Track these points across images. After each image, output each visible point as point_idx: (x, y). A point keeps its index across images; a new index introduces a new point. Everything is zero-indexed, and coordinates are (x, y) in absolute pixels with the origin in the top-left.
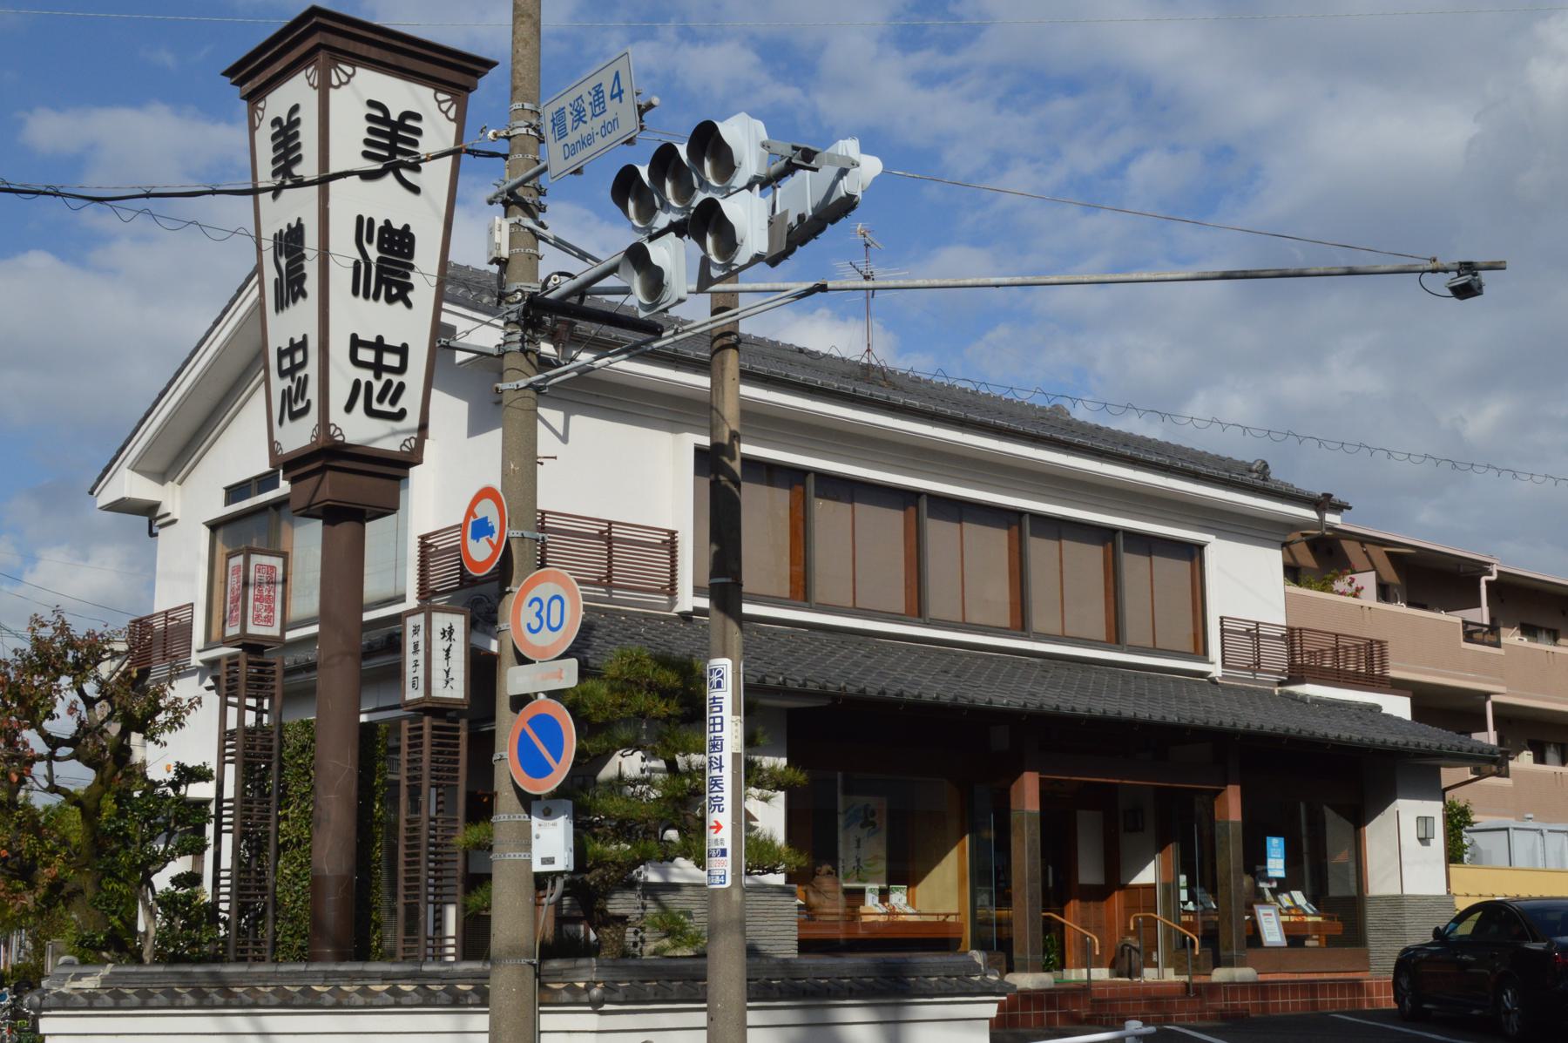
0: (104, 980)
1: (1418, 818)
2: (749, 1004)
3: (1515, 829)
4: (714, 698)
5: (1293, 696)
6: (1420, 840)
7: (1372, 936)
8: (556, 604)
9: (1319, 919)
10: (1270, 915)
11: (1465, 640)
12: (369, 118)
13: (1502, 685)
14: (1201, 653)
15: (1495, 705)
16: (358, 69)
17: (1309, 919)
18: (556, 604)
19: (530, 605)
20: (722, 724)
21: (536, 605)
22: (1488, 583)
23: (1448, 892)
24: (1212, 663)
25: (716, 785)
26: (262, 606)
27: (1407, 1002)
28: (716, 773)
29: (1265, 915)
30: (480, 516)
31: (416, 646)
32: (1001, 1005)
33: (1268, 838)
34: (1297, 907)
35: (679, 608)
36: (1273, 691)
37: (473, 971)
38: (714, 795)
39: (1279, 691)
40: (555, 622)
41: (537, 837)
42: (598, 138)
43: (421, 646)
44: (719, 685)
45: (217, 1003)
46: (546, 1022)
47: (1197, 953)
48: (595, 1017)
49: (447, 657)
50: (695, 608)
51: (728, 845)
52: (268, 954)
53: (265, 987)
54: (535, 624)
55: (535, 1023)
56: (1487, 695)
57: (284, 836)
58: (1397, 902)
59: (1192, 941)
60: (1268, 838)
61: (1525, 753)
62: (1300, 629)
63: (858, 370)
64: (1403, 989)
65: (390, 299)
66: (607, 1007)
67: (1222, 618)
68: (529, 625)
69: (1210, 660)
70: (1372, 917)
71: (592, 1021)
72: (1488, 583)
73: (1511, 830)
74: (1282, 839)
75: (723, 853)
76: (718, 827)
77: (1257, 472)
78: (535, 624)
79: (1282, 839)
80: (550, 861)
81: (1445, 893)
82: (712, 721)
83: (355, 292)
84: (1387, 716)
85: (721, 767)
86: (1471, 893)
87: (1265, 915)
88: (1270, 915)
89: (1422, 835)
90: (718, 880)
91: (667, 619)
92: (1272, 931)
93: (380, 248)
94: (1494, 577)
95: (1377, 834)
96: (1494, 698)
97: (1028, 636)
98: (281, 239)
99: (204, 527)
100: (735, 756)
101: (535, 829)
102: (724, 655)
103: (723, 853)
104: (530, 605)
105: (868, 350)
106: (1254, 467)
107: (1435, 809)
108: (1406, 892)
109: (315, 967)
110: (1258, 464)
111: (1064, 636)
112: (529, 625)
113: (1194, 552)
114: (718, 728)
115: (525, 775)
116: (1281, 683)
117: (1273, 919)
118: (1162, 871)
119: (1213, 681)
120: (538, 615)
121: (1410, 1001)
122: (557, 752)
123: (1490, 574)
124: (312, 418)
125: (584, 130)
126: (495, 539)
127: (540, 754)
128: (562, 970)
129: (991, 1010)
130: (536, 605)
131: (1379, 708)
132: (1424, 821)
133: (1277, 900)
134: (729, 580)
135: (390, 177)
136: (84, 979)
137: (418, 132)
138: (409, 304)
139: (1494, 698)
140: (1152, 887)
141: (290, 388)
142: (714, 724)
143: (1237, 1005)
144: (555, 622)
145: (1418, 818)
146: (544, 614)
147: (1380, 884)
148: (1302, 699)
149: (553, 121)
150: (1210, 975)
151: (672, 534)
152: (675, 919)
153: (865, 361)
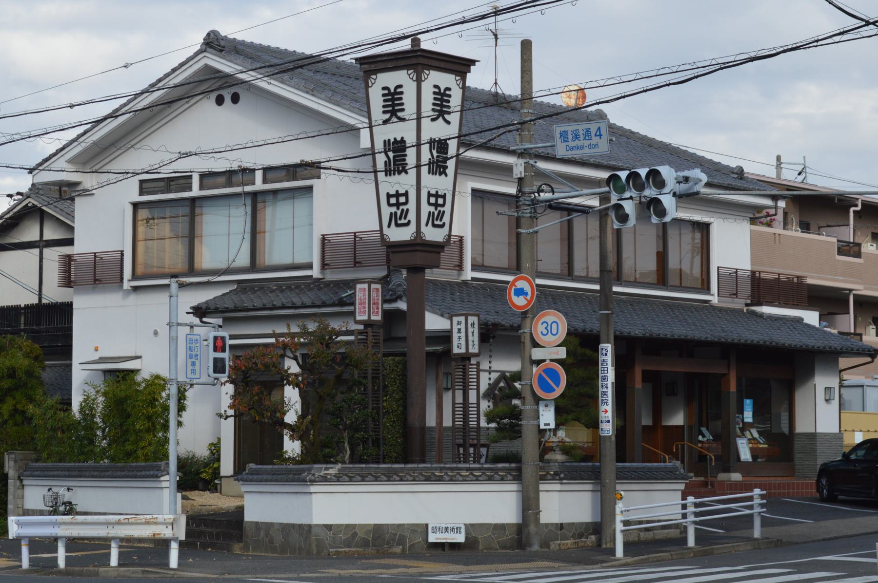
0: (339, 470)
1: (826, 388)
2: (617, 481)
3: (868, 386)
4: (604, 360)
5: (754, 313)
6: (827, 400)
7: (797, 456)
8: (554, 325)
9: (766, 446)
10: (744, 443)
11: (838, 255)
12: (435, 93)
13: (861, 284)
14: (707, 289)
15: (855, 295)
16: (431, 71)
17: (761, 446)
18: (554, 325)
19: (542, 324)
20: (607, 370)
21: (545, 325)
22: (854, 212)
23: (840, 431)
24: (713, 295)
25: (605, 394)
26: (375, 306)
27: (825, 491)
28: (605, 390)
29: (741, 443)
30: (519, 287)
31: (459, 331)
32: (687, 485)
33: (745, 400)
34: (754, 439)
35: (464, 278)
36: (743, 310)
37: (505, 467)
38: (604, 399)
39: (747, 310)
40: (554, 332)
41: (542, 415)
42: (587, 149)
43: (463, 330)
44: (606, 354)
45: (382, 480)
46: (542, 487)
47: (713, 464)
48: (559, 485)
49: (473, 335)
50: (472, 278)
51: (610, 419)
52: (381, 460)
53: (414, 473)
54: (545, 332)
55: (538, 487)
56: (851, 290)
57: (385, 409)
58: (812, 437)
59: (711, 459)
60: (745, 400)
61: (871, 327)
62: (760, 272)
63: (491, 98)
64: (823, 485)
65: (440, 174)
66: (564, 481)
67: (718, 268)
68: (542, 332)
69: (711, 293)
70: (797, 445)
71: (558, 487)
72: (854, 212)
73: (865, 387)
74: (752, 400)
75: (608, 422)
76: (606, 411)
77: (737, 174)
78: (545, 332)
79: (752, 400)
80: (548, 425)
81: (838, 431)
82: (603, 369)
83: (429, 173)
84: (807, 325)
85: (607, 388)
86: (848, 430)
87: (741, 443)
88: (744, 443)
89: (828, 398)
90: (606, 432)
91: (457, 284)
92: (745, 454)
93: (437, 152)
94: (859, 208)
95: (801, 397)
96: (854, 292)
97: (621, 284)
98: (389, 145)
99: (130, 204)
100: (612, 383)
101: (541, 412)
102: (608, 342)
103: (608, 422)
104: (542, 324)
105: (496, 83)
106: (736, 171)
107: (834, 382)
108: (818, 431)
109: (410, 466)
110: (738, 169)
111: (483, 266)
112: (542, 332)
113: (704, 228)
114: (606, 372)
115: (541, 391)
116: (747, 305)
117: (745, 445)
118: (688, 417)
119: (714, 308)
120: (546, 328)
121: (827, 491)
122: (558, 383)
123: (856, 206)
124: (412, 228)
125: (577, 143)
126: (529, 297)
127: (549, 384)
128: (544, 467)
129: (682, 487)
130: (545, 325)
131: (802, 319)
132: (828, 389)
133: (743, 435)
134: (610, 312)
135: (441, 119)
136: (330, 470)
137: (450, 96)
138: (446, 175)
139: (854, 292)
140: (682, 427)
141: (396, 213)
142: (604, 370)
143: (89, 570)
144: (554, 332)
145: (826, 388)
146: (549, 328)
147: (802, 426)
148: (761, 316)
149: (560, 134)
150: (716, 477)
151: (462, 237)
152: (92, 429)
153: (493, 90)
